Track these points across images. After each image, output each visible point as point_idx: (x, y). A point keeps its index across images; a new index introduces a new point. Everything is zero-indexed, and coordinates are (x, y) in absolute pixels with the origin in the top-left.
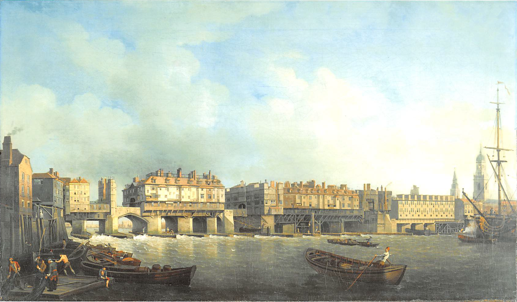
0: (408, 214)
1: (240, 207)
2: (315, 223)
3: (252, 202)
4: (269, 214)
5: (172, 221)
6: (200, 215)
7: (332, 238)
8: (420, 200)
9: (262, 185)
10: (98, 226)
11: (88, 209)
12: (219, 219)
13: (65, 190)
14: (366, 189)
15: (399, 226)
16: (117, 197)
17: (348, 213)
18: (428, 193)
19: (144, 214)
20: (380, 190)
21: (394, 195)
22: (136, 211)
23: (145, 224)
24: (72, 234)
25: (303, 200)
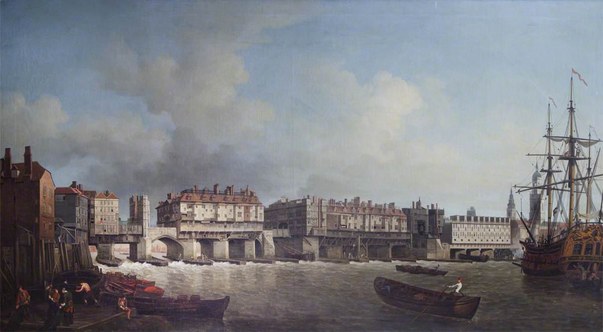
0: (462, 236)
1: (280, 227)
2: (361, 246)
3: (295, 220)
4: (311, 235)
5: (207, 242)
6: (236, 236)
7: (405, 263)
8: (50, 244)
9: (304, 200)
10: (129, 250)
11: (116, 231)
12: (257, 242)
13: (90, 206)
14: (415, 207)
15: (453, 252)
16: (150, 216)
17: (394, 237)
18: (485, 215)
19: (181, 236)
20: (430, 208)
21: (447, 215)
22: (172, 232)
23: (180, 249)
24: (98, 260)
25: (349, 221)
